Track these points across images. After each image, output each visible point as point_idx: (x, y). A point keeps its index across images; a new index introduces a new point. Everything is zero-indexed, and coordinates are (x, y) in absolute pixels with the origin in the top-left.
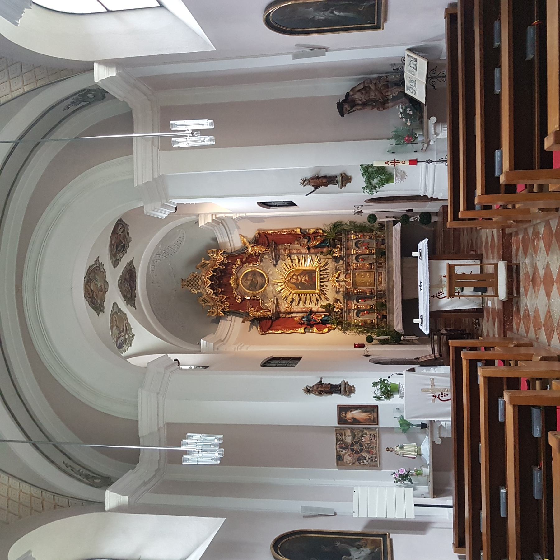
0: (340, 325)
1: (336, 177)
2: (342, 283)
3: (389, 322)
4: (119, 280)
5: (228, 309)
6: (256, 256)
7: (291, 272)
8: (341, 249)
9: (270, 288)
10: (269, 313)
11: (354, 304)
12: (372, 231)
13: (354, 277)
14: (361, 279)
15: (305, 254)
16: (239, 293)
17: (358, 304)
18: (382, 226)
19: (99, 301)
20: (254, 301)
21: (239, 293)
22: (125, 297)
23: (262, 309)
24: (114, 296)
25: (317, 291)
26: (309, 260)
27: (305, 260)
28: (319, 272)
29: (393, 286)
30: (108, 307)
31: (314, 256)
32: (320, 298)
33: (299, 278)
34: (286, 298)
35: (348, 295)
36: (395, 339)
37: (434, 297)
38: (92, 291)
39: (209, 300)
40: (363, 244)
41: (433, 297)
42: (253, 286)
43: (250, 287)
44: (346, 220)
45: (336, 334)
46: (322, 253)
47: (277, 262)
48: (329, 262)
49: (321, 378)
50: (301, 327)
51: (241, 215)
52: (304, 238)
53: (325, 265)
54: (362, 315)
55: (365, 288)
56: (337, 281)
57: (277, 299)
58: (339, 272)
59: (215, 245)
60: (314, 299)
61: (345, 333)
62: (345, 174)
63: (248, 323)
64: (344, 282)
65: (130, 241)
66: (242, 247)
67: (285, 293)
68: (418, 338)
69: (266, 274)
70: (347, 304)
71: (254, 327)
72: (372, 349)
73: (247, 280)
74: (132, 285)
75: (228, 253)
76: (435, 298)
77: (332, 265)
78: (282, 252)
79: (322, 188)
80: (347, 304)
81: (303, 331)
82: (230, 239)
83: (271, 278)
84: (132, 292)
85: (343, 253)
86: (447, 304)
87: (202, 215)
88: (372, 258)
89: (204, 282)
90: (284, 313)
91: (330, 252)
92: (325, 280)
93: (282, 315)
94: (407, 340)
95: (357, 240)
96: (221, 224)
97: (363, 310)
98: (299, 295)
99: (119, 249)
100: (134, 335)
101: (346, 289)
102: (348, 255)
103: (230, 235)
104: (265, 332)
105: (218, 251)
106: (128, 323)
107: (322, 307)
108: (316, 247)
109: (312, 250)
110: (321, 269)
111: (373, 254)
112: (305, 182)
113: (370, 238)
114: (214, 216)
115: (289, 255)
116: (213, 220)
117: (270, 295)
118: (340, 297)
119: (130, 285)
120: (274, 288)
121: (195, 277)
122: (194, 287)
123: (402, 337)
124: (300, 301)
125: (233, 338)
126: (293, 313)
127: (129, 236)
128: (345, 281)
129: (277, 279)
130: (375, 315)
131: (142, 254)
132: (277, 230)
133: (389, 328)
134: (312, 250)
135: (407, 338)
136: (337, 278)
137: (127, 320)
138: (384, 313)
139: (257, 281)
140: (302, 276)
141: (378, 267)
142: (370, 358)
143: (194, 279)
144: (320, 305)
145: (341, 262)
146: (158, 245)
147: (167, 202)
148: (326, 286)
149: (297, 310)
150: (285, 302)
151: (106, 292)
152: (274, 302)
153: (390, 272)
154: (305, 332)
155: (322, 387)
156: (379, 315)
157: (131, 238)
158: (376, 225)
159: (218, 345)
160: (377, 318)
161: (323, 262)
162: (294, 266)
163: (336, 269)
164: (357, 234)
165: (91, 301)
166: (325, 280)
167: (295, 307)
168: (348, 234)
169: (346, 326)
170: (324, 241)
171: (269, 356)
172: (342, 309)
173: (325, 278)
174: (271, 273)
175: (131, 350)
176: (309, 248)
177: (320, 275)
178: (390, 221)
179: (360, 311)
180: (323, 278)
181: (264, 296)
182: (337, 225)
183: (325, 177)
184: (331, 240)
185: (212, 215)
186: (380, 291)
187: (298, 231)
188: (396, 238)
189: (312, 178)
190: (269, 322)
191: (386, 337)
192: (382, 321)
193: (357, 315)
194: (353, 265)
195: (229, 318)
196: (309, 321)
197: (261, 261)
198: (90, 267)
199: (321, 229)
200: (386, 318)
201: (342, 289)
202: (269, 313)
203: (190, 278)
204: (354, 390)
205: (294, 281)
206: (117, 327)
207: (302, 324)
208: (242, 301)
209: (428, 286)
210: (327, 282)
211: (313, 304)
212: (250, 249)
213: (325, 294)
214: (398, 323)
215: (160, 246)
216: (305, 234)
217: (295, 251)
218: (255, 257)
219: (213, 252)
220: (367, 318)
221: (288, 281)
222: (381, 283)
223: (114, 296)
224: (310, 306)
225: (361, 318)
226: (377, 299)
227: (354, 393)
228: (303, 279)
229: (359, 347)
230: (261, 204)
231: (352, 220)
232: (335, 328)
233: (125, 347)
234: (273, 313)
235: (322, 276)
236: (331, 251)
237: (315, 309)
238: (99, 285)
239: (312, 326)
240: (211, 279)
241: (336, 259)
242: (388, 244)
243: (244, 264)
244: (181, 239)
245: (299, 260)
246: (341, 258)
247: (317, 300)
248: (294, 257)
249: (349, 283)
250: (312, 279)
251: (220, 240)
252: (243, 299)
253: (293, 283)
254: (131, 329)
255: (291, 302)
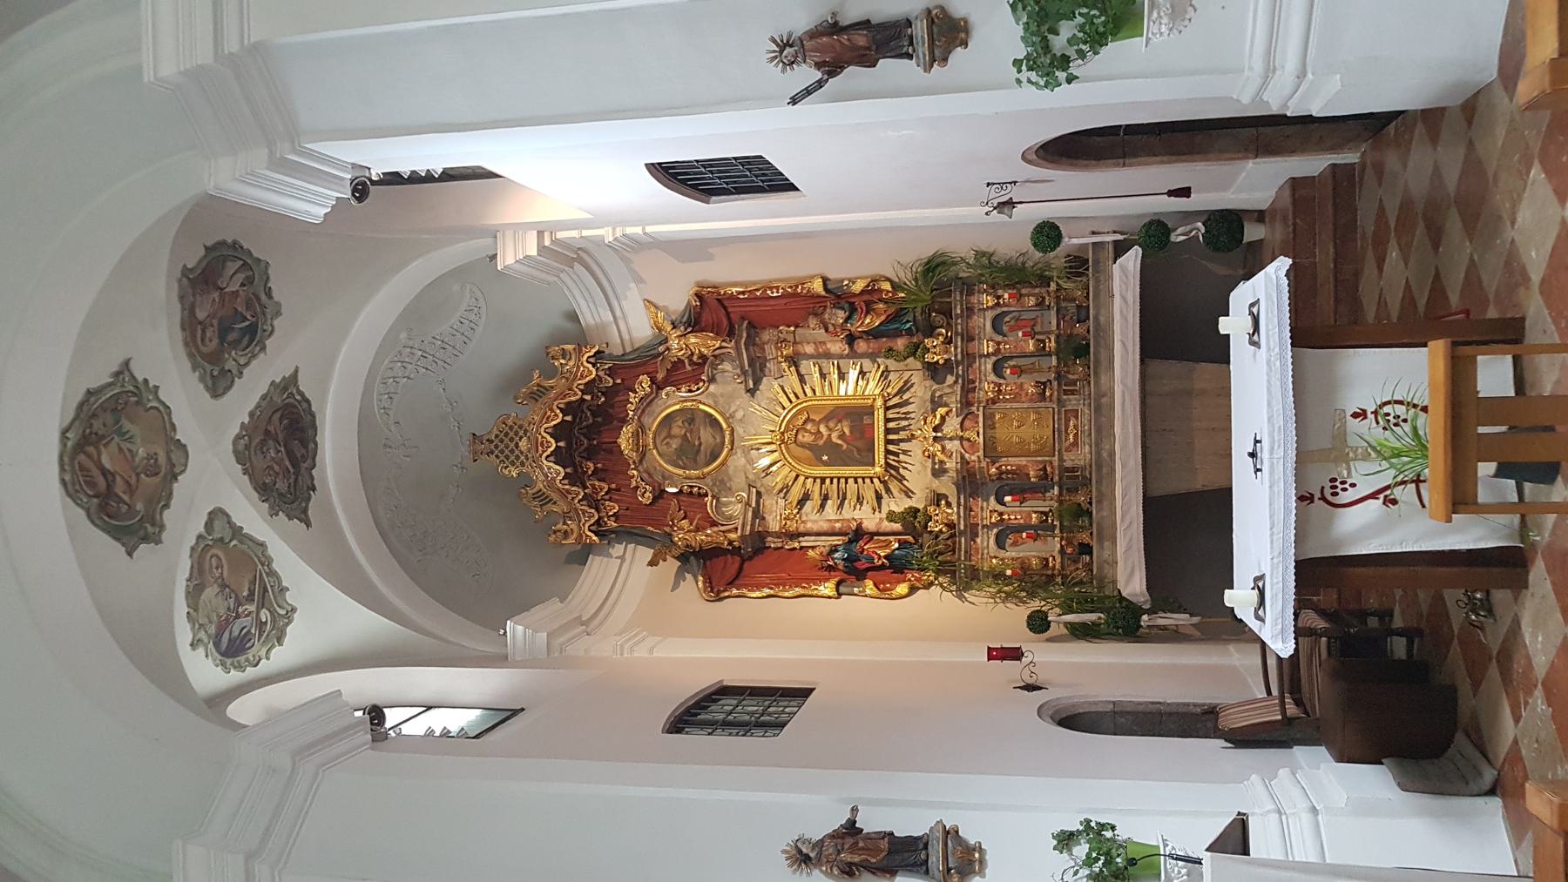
0: (945, 573)
1: (909, 23)
2: (953, 446)
3: (1100, 568)
4: (238, 437)
5: (612, 524)
6: (692, 363)
7: (799, 412)
8: (948, 341)
9: (738, 460)
10: (733, 536)
11: (987, 509)
12: (1045, 281)
13: (989, 425)
14: (1007, 433)
15: (841, 357)
16: (645, 476)
17: (1001, 508)
18: (1078, 265)
19: (139, 506)
20: (692, 498)
21: (645, 476)
22: (264, 490)
23: (714, 524)
24: (213, 483)
25: (878, 469)
26: (853, 374)
27: (842, 376)
28: (881, 411)
29: (1112, 454)
30: (184, 523)
31: (867, 364)
32: (888, 490)
33: (823, 429)
34: (786, 489)
35: (970, 483)
36: (1123, 623)
37: (1315, 497)
38: (104, 472)
39: (555, 496)
40: (1019, 323)
41: (1311, 498)
42: (689, 454)
43: (679, 457)
44: (961, 248)
45: (933, 604)
46: (889, 353)
47: (757, 382)
48: (914, 380)
49: (854, 810)
50: (827, 580)
51: (630, 230)
52: (836, 306)
53: (901, 392)
54: (1015, 544)
55: (1023, 461)
56: (935, 439)
57: (759, 494)
58: (942, 411)
59: (575, 334)
60: (869, 495)
61: (961, 597)
62: (942, 9)
63: (672, 565)
64: (957, 443)
65: (278, 313)
66: (655, 337)
67: (782, 474)
68: (1196, 620)
69: (726, 420)
70: (969, 509)
71: (688, 576)
72: (1045, 656)
73: (669, 436)
74: (299, 451)
75: (611, 357)
76: (1318, 503)
77: (922, 388)
78: (770, 351)
79: (853, 74)
80: (969, 509)
81: (832, 592)
82: (618, 313)
83: (739, 430)
84: (297, 474)
85: (954, 353)
86: (1363, 529)
87: (509, 234)
88: (1045, 366)
89: (536, 445)
90: (778, 535)
91: (915, 350)
92: (903, 435)
93: (772, 543)
94: (1164, 628)
95: (999, 311)
96: (577, 265)
97: (1018, 529)
98: (823, 480)
99: (232, 336)
100: (294, 610)
101: (964, 462)
102: (969, 358)
103: (615, 304)
104: (719, 592)
105: (579, 352)
106: (273, 574)
107: (891, 517)
108: (874, 334)
109: (861, 346)
110: (890, 403)
111: (1050, 355)
112: (788, 50)
113: (1040, 304)
114: (547, 235)
115: (794, 361)
116: (542, 249)
117: (739, 481)
118: (946, 486)
119: (290, 454)
120: (751, 462)
121: (511, 428)
122: (507, 457)
123: (1145, 617)
124: (826, 498)
125: (626, 608)
126: (804, 535)
127: (270, 297)
128: (961, 438)
129: (760, 433)
130: (1056, 544)
131: (334, 353)
132: (754, 283)
133: (1101, 587)
134: (861, 346)
135: (1161, 622)
136: (935, 429)
137: (268, 561)
138: (1084, 537)
139: (701, 441)
140: (831, 424)
141: (1066, 392)
142: (1038, 697)
143: (506, 435)
144: (885, 510)
145: (950, 379)
146: (393, 331)
147: (295, 152)
148: (905, 452)
149: (815, 528)
150: (781, 502)
151: (175, 477)
152: (748, 504)
153: (1102, 410)
154: (840, 595)
155: (854, 849)
156: (1069, 543)
157: (278, 304)
158: (1057, 257)
159: (562, 640)
160: (1062, 551)
161: (896, 382)
162: (808, 391)
163: (932, 401)
164: (1000, 292)
165: (103, 508)
166: (903, 435)
167: (812, 518)
168: (970, 293)
169: (964, 578)
170: (891, 319)
171: (705, 681)
172: (951, 526)
173: (903, 429)
174: (739, 415)
175: (280, 657)
176: (851, 339)
177: (887, 420)
178: (1102, 243)
179: (1008, 533)
180: (896, 431)
181: (722, 486)
182: (935, 268)
183: (865, 24)
184: (919, 310)
185: (540, 234)
186: (1073, 470)
187: (817, 287)
188: (1124, 299)
189: (813, 34)
190: (734, 563)
191: (1092, 617)
192: (1076, 561)
193: (1000, 544)
194: (986, 389)
195: (618, 549)
196: (851, 560)
197: (712, 380)
198: (89, 393)
199: (888, 279)
200: (1091, 554)
201: (951, 465)
202: (733, 536)
203: (495, 432)
204: (982, 862)
205: (806, 438)
206: (224, 586)
207: (830, 568)
208: (655, 499)
209: (1292, 454)
210: (908, 440)
211: (866, 508)
212: (674, 344)
213: (901, 479)
214: (1132, 573)
215: (403, 336)
216: (837, 295)
217: (809, 349)
218: (689, 368)
219: (564, 354)
220: (1029, 551)
221: (787, 439)
222: (1075, 444)
223: (213, 483)
224: (857, 514)
225: (1011, 553)
226: (1061, 494)
227: (981, 873)
228: (835, 433)
229: (1003, 659)
230: (671, 174)
231: (984, 248)
232: (931, 584)
233: (258, 649)
234: (743, 537)
235: (891, 425)
236: (917, 346)
237: (870, 524)
238: (141, 452)
239: (860, 576)
240: (557, 433)
241: (935, 372)
242: (1096, 318)
243: (660, 388)
244: (473, 317)
245: (823, 376)
246: (948, 366)
247: (879, 497)
248: (810, 368)
249: (973, 443)
250: (862, 433)
251: (588, 317)
252: (660, 494)
253: (803, 446)
254: (283, 590)
255: (801, 503)
